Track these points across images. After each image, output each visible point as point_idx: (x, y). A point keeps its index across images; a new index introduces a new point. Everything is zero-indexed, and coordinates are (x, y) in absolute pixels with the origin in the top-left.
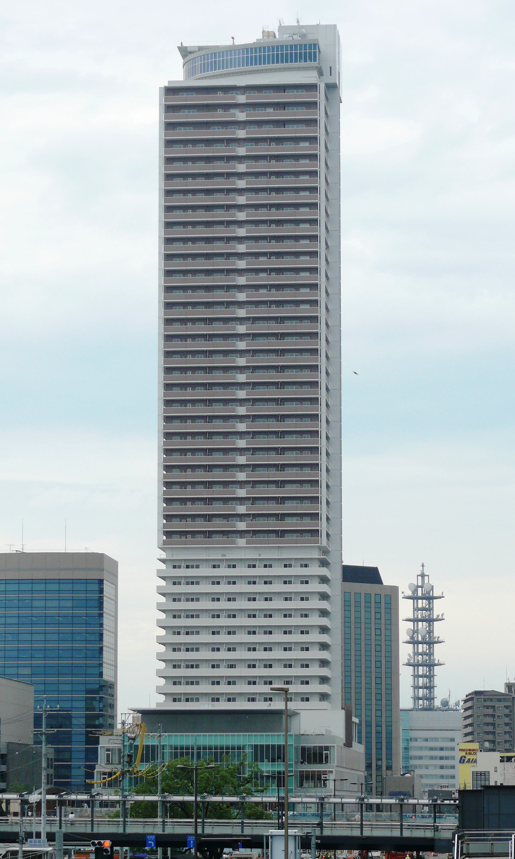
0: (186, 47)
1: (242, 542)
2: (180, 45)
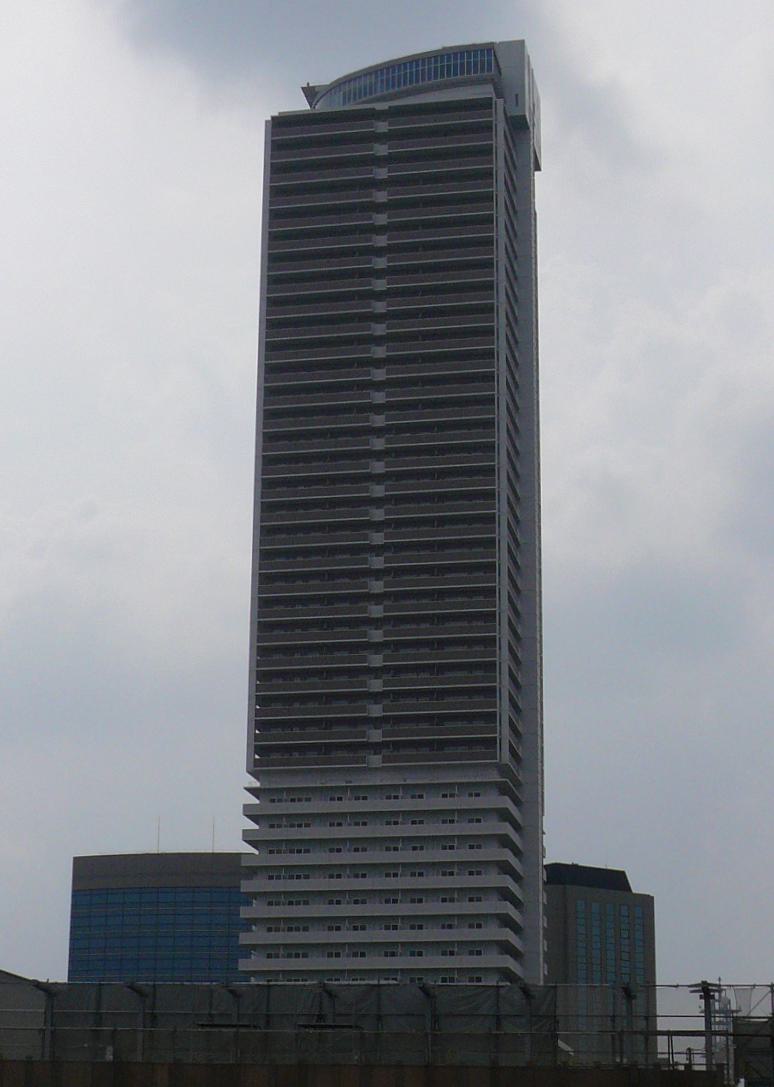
0: (314, 87)
1: (375, 760)
2: (305, 85)
